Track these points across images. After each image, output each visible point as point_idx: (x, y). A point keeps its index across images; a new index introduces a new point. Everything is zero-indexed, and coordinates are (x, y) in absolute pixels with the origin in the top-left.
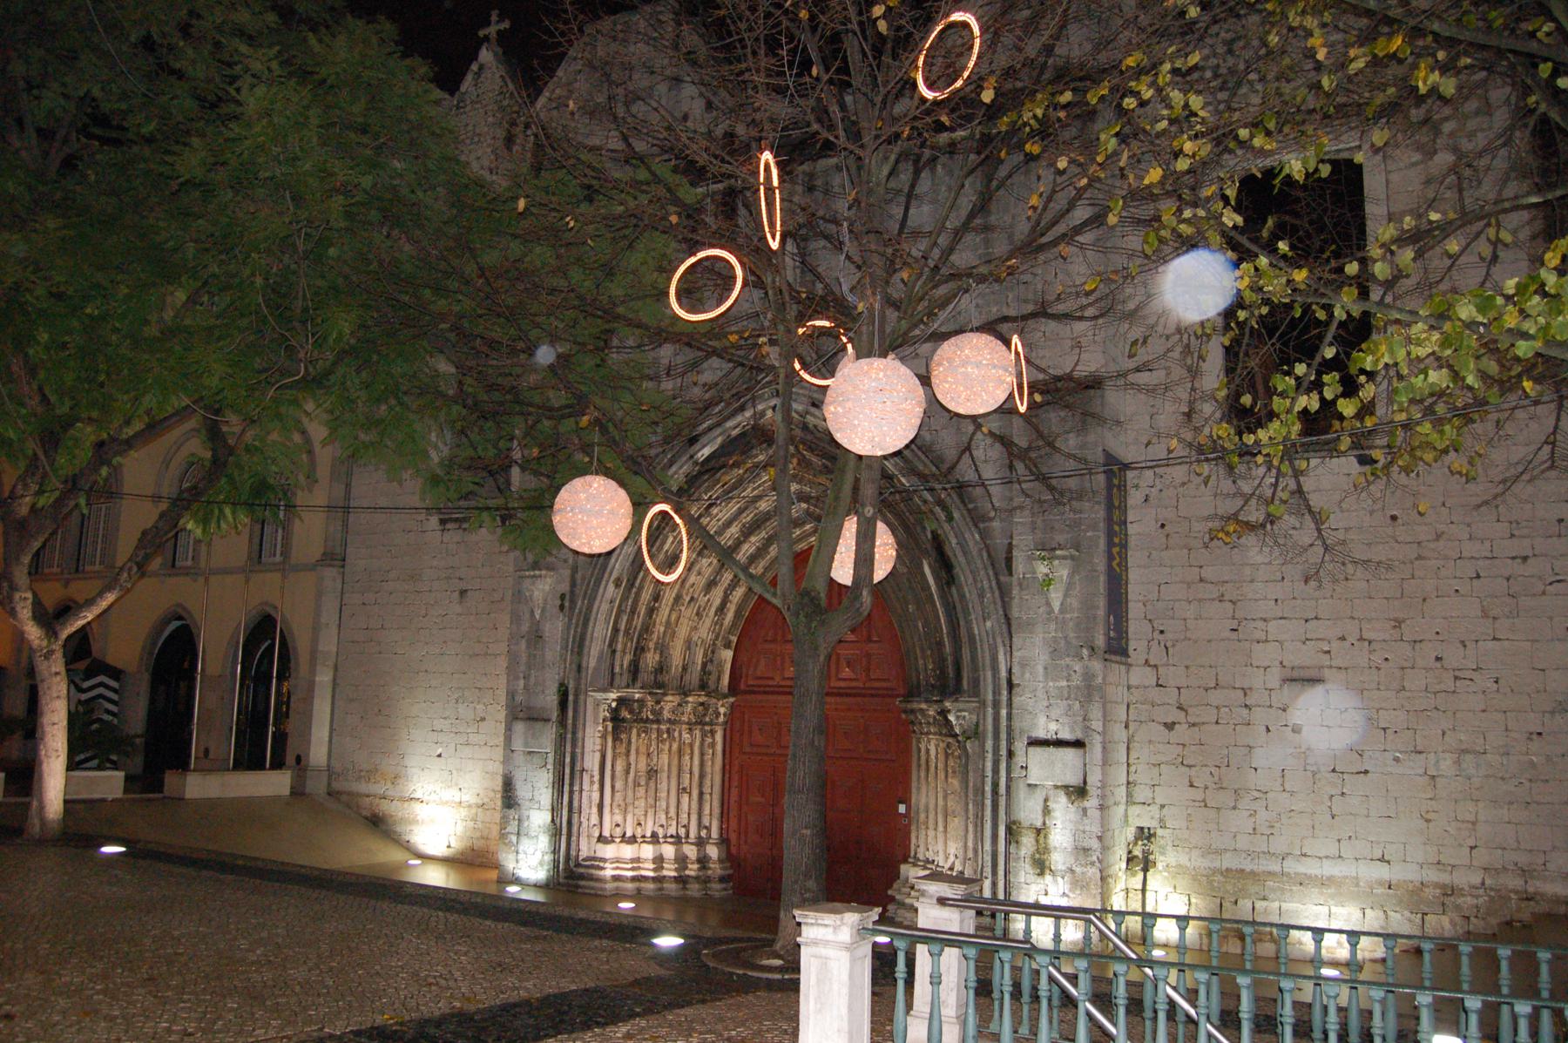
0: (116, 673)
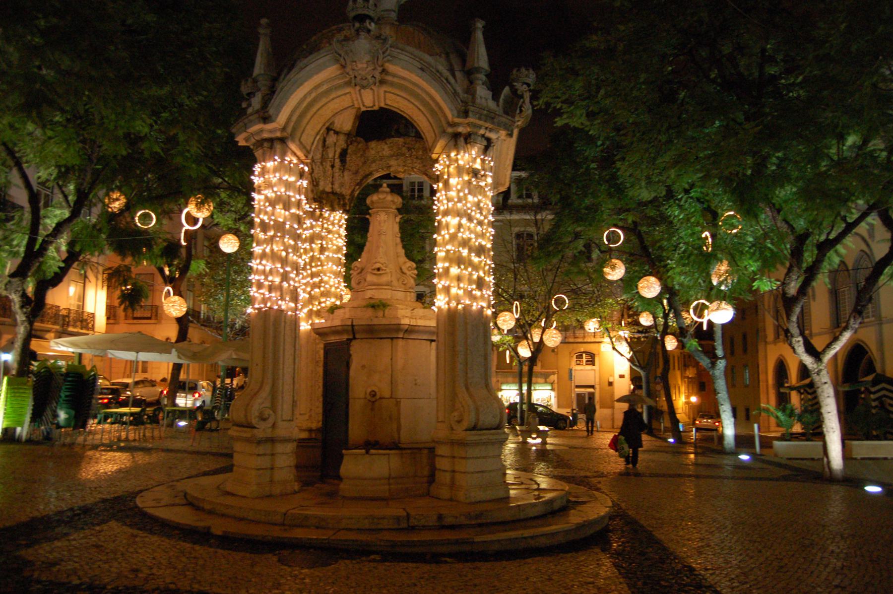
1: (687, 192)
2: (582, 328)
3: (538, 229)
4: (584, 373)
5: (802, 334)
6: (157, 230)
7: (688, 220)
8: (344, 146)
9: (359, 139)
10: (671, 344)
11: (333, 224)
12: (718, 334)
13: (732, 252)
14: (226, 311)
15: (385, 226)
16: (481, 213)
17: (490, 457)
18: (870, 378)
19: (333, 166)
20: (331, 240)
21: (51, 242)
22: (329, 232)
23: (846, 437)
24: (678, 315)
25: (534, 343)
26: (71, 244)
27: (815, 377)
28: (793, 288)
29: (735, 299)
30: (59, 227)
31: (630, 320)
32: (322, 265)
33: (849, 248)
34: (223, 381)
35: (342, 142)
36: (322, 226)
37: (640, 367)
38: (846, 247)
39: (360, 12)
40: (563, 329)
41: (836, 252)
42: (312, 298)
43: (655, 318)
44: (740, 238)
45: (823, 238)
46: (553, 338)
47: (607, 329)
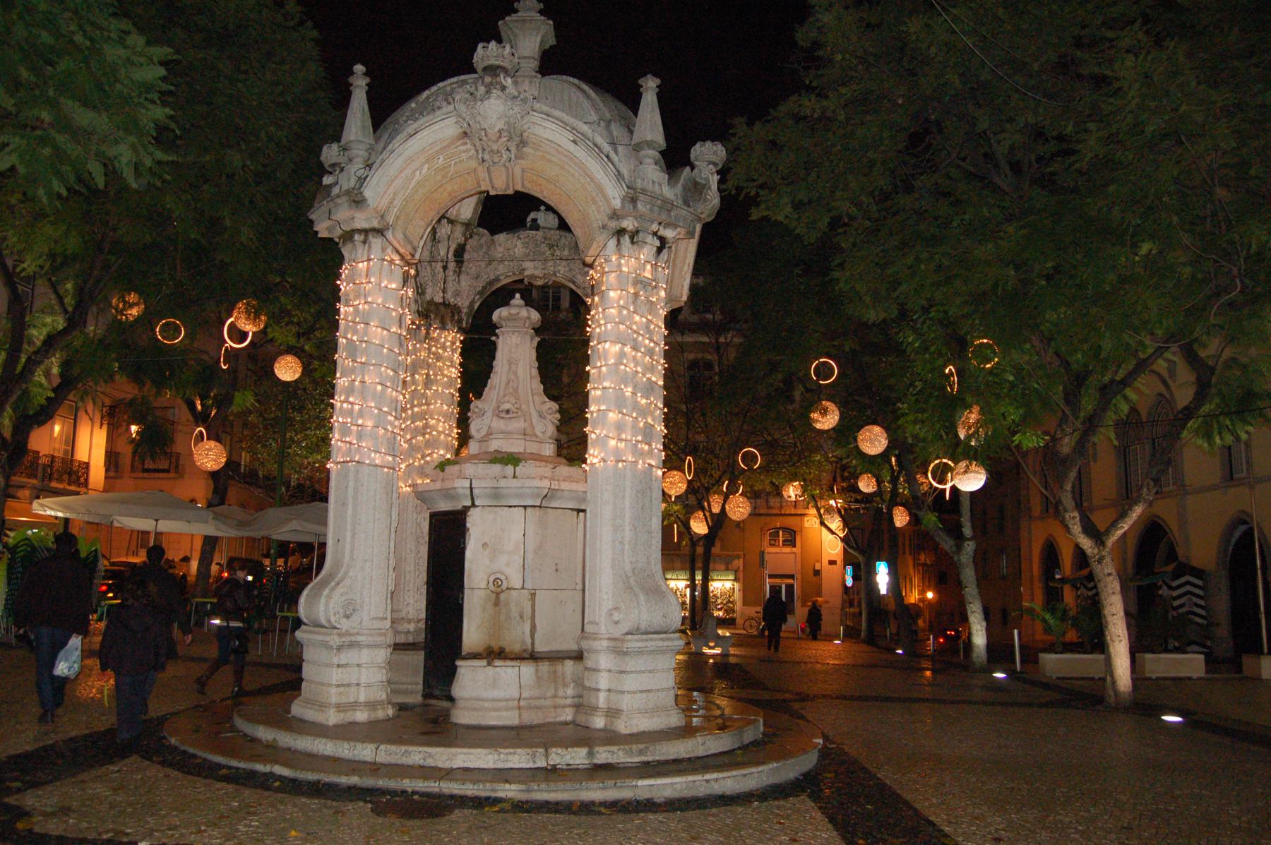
0: (1199, 573)
1: (926, 310)
2: (779, 494)
3: (720, 357)
4: (780, 557)
5: (1079, 506)
6: (183, 350)
7: (927, 349)
8: (461, 240)
9: (481, 230)
10: (901, 518)
11: (444, 347)
12: (966, 505)
13: (978, 389)
14: (281, 465)
15: (516, 350)
16: (651, 340)
17: (658, 671)
18: (1170, 568)
19: (445, 268)
20: (440, 369)
21: (40, 363)
22: (439, 358)
23: (1135, 651)
24: (911, 480)
25: (712, 514)
26: (66, 365)
27: (1097, 568)
28: (1066, 445)
29: (989, 458)
30: (51, 342)
31: (844, 484)
32: (428, 404)
33: (1142, 393)
34: (273, 563)
35: (458, 236)
36: (429, 349)
37: (857, 549)
38: (1137, 390)
39: (493, 62)
40: (753, 495)
41: (1126, 398)
42: (414, 448)
43: (879, 482)
44: (997, 375)
45: (1107, 379)
46: (739, 508)
47: (813, 497)
